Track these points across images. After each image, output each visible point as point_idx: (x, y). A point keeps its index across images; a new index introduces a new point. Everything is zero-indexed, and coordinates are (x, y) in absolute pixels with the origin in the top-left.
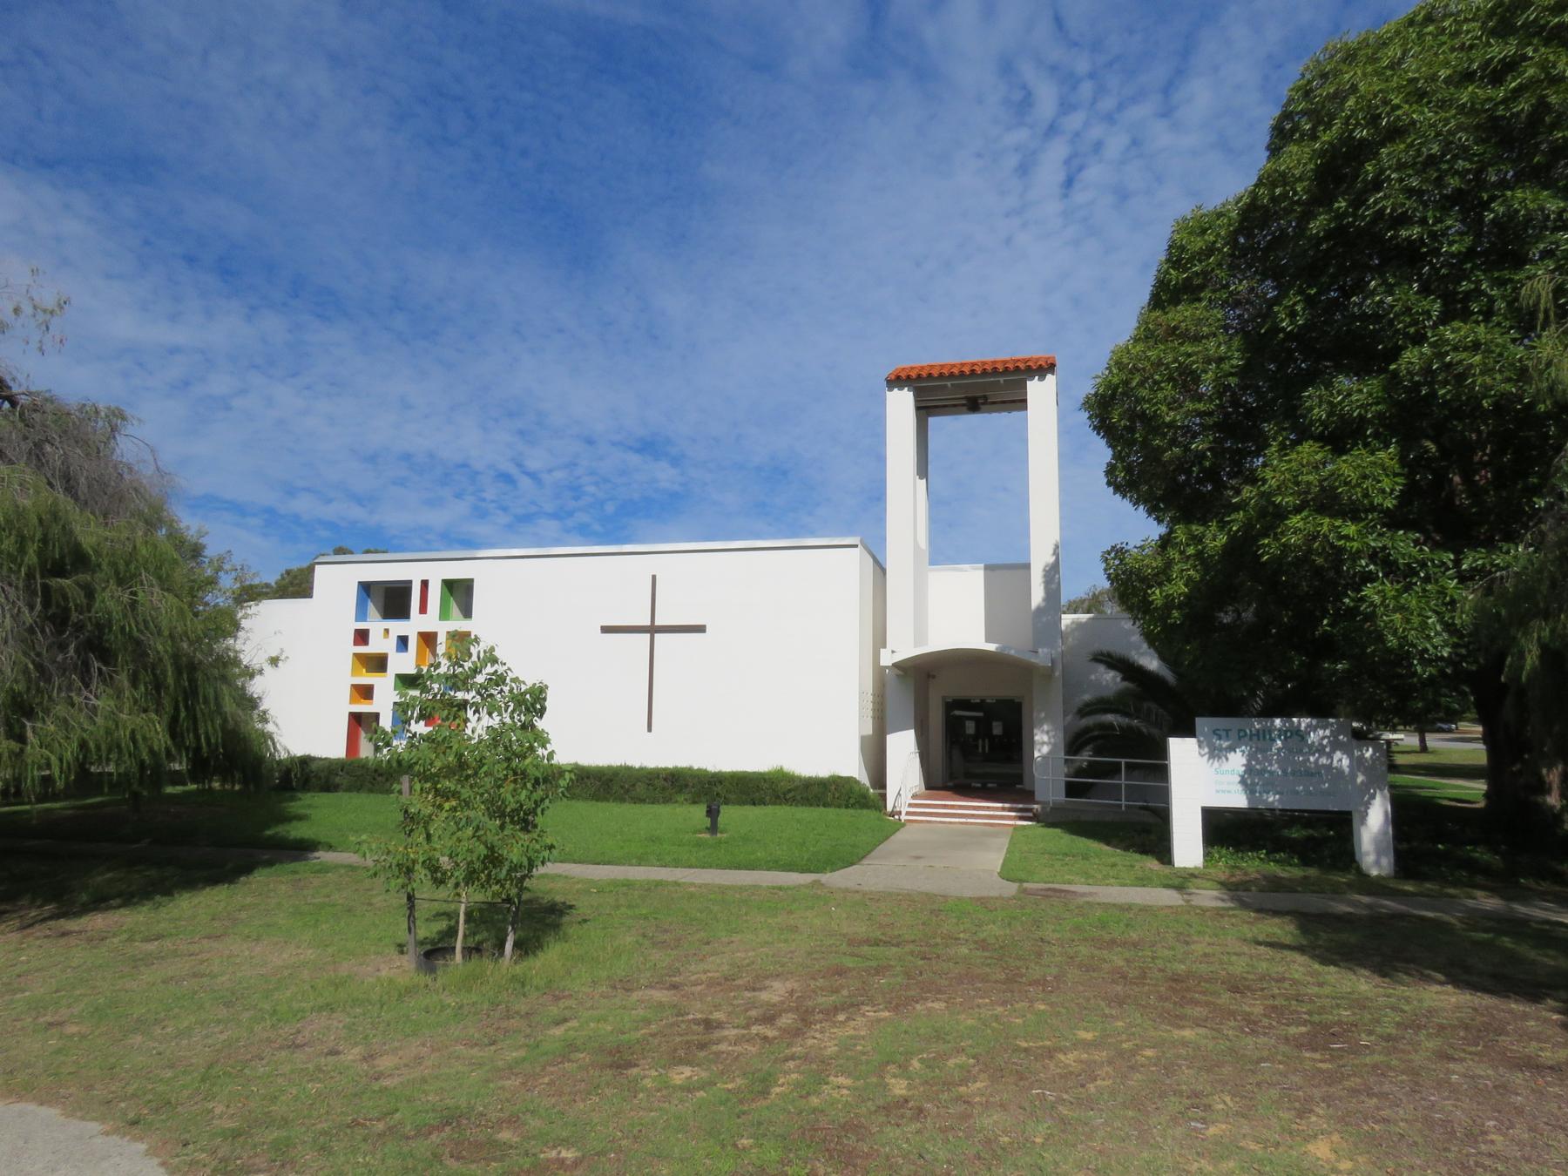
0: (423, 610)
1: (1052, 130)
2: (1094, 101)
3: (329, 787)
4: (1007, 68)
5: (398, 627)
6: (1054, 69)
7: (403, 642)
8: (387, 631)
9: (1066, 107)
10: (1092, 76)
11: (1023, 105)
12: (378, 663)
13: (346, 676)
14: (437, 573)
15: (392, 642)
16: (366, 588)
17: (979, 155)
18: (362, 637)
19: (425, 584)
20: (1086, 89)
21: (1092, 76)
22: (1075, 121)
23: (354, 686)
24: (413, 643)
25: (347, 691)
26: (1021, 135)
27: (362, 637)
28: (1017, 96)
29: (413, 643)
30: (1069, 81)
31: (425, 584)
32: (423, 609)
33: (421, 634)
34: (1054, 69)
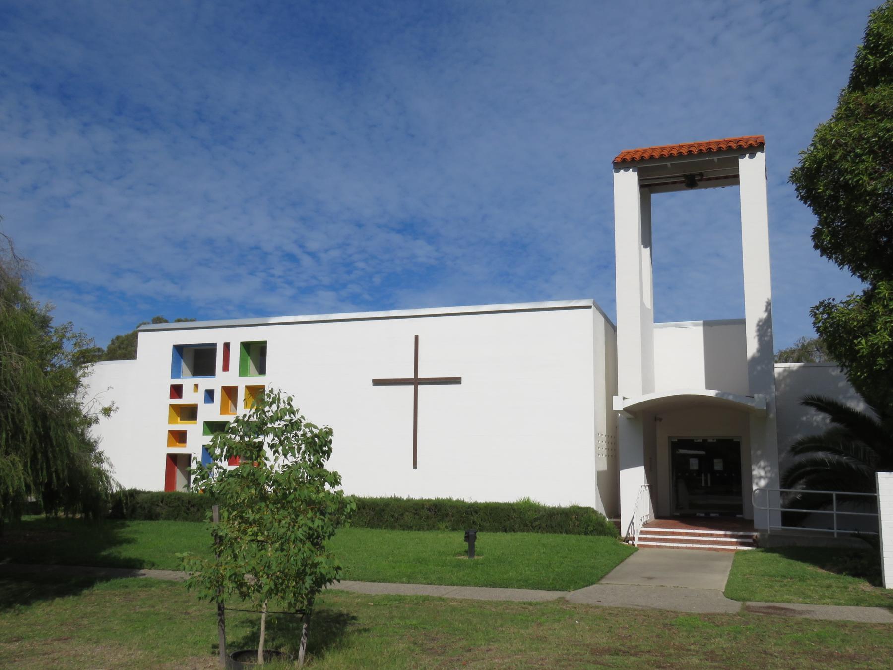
0: (226, 367)
5: (205, 382)
7: (210, 394)
8: (197, 386)
12: (190, 413)
15: (201, 394)
16: (179, 350)
18: (176, 391)
19: (227, 346)
27: (176, 391)
31: (227, 346)
32: (226, 367)
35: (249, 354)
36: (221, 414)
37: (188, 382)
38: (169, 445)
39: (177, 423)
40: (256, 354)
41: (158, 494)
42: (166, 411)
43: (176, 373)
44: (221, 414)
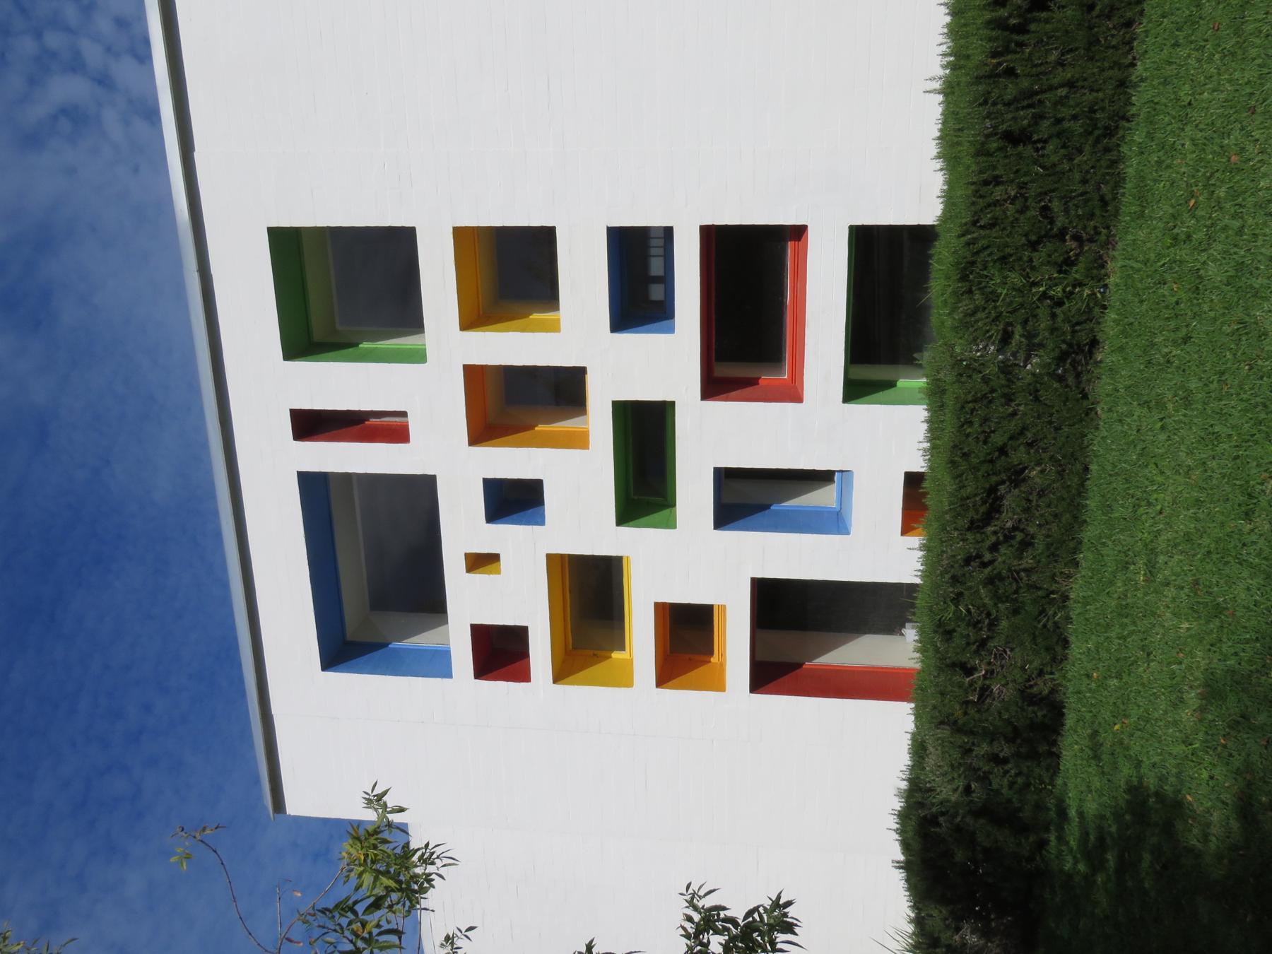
0: (388, 428)
1: (104, 80)
2: (68, 30)
3: (1038, 728)
4: (32, 140)
5: (462, 525)
6: (33, 82)
7: (513, 501)
8: (480, 562)
9: (76, 65)
10: (38, 35)
11: (76, 119)
12: (590, 593)
13: (631, 702)
14: (264, 381)
15: (508, 538)
16: (340, 649)
17: (136, 170)
18: (499, 652)
19: (309, 425)
20: (54, 40)
21: (38, 35)
22: (93, 54)
23: (665, 677)
24: (511, 461)
25: (679, 699)
26: (110, 117)
27: (499, 652)
28: (65, 125)
29: (511, 461)
30: (45, 64)
31: (309, 425)
32: (388, 428)
33: (477, 437)
34: (33, 82)
35: (767, 507)
36: (288, 246)
37: (470, 602)
38: (717, 684)
39: (629, 663)
40: (345, 286)
41: (918, 716)
42: (581, 697)
43: (437, 664)
44: (288, 246)
